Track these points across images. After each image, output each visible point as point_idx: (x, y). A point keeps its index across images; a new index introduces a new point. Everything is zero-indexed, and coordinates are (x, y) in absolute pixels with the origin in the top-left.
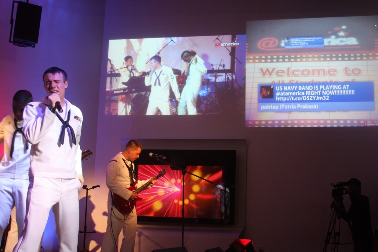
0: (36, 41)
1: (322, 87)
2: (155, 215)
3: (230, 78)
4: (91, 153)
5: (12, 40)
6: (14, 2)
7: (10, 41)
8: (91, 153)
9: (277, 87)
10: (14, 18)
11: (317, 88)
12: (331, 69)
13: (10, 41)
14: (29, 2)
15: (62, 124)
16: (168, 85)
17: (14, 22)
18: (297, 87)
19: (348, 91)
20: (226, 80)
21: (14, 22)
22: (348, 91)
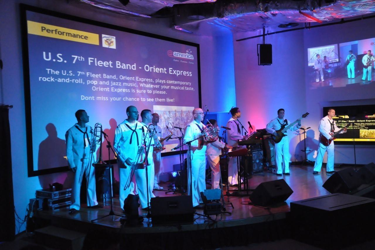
0: (271, 63)
1: (113, 84)
2: (367, 83)
3: (339, 65)
4: (309, 114)
5: (259, 64)
6: (258, 45)
7: (259, 65)
8: (309, 114)
9: (84, 60)
10: (259, 53)
11: (191, 75)
12: (95, 126)
13: (259, 65)
14: (265, 43)
15: (197, 149)
16: (137, 167)
17: (259, 55)
18: (175, 71)
19: (81, 82)
20: (331, 59)
21: (259, 55)
22: (81, 82)
